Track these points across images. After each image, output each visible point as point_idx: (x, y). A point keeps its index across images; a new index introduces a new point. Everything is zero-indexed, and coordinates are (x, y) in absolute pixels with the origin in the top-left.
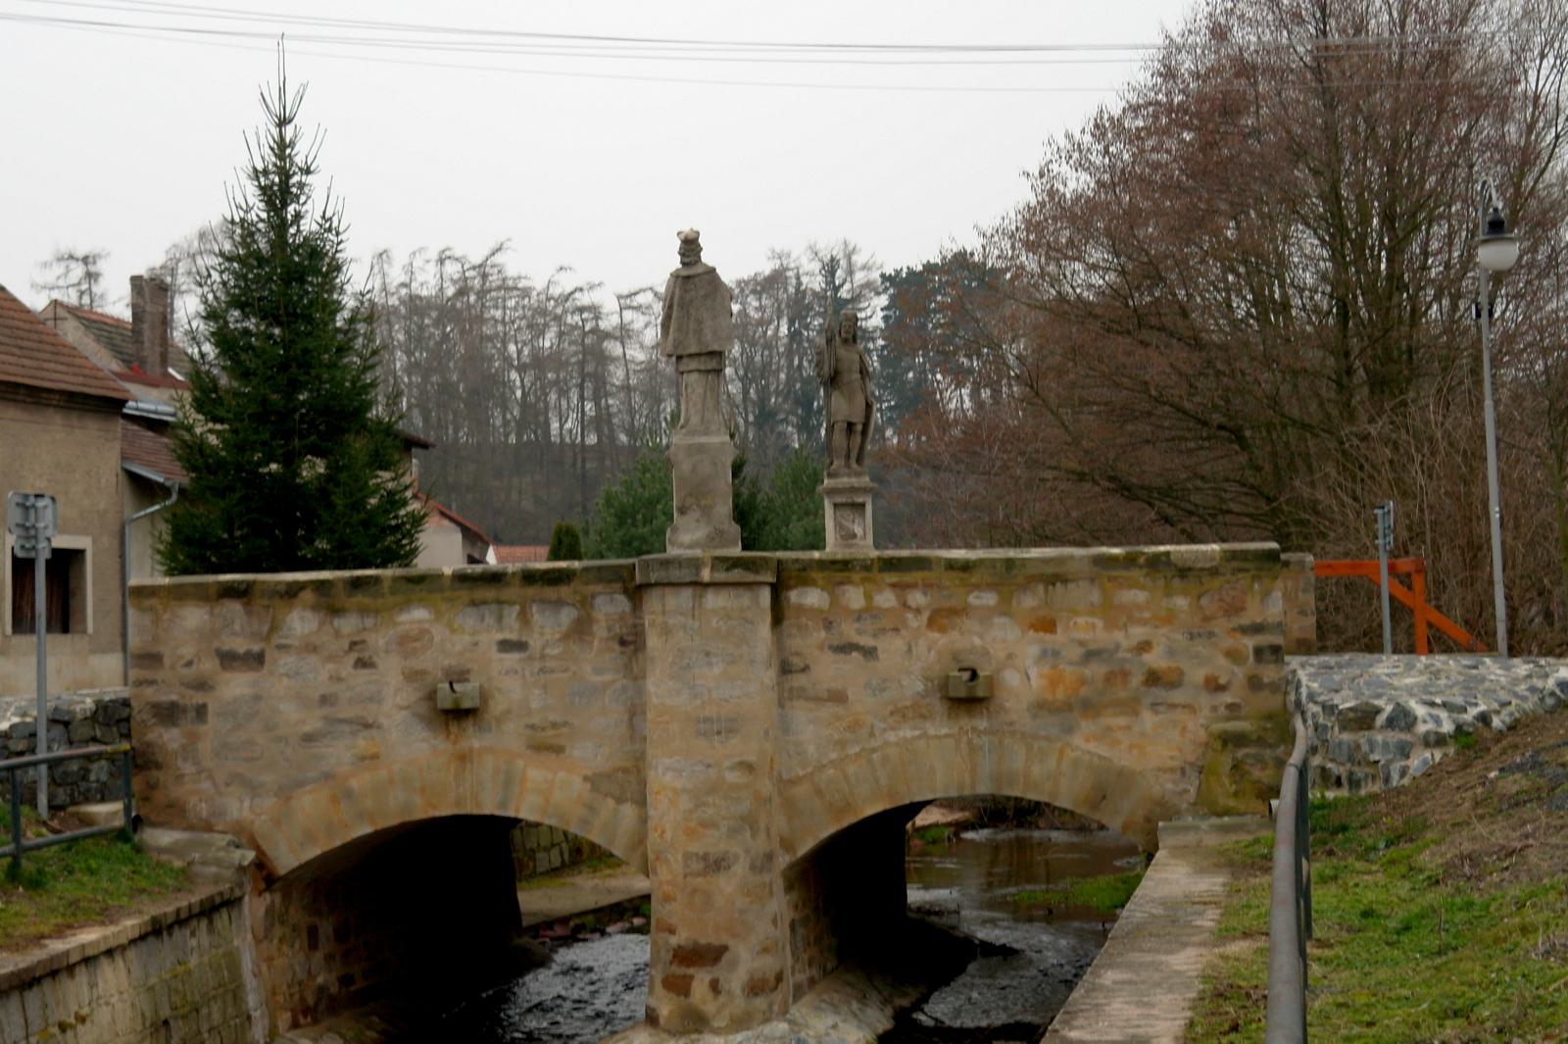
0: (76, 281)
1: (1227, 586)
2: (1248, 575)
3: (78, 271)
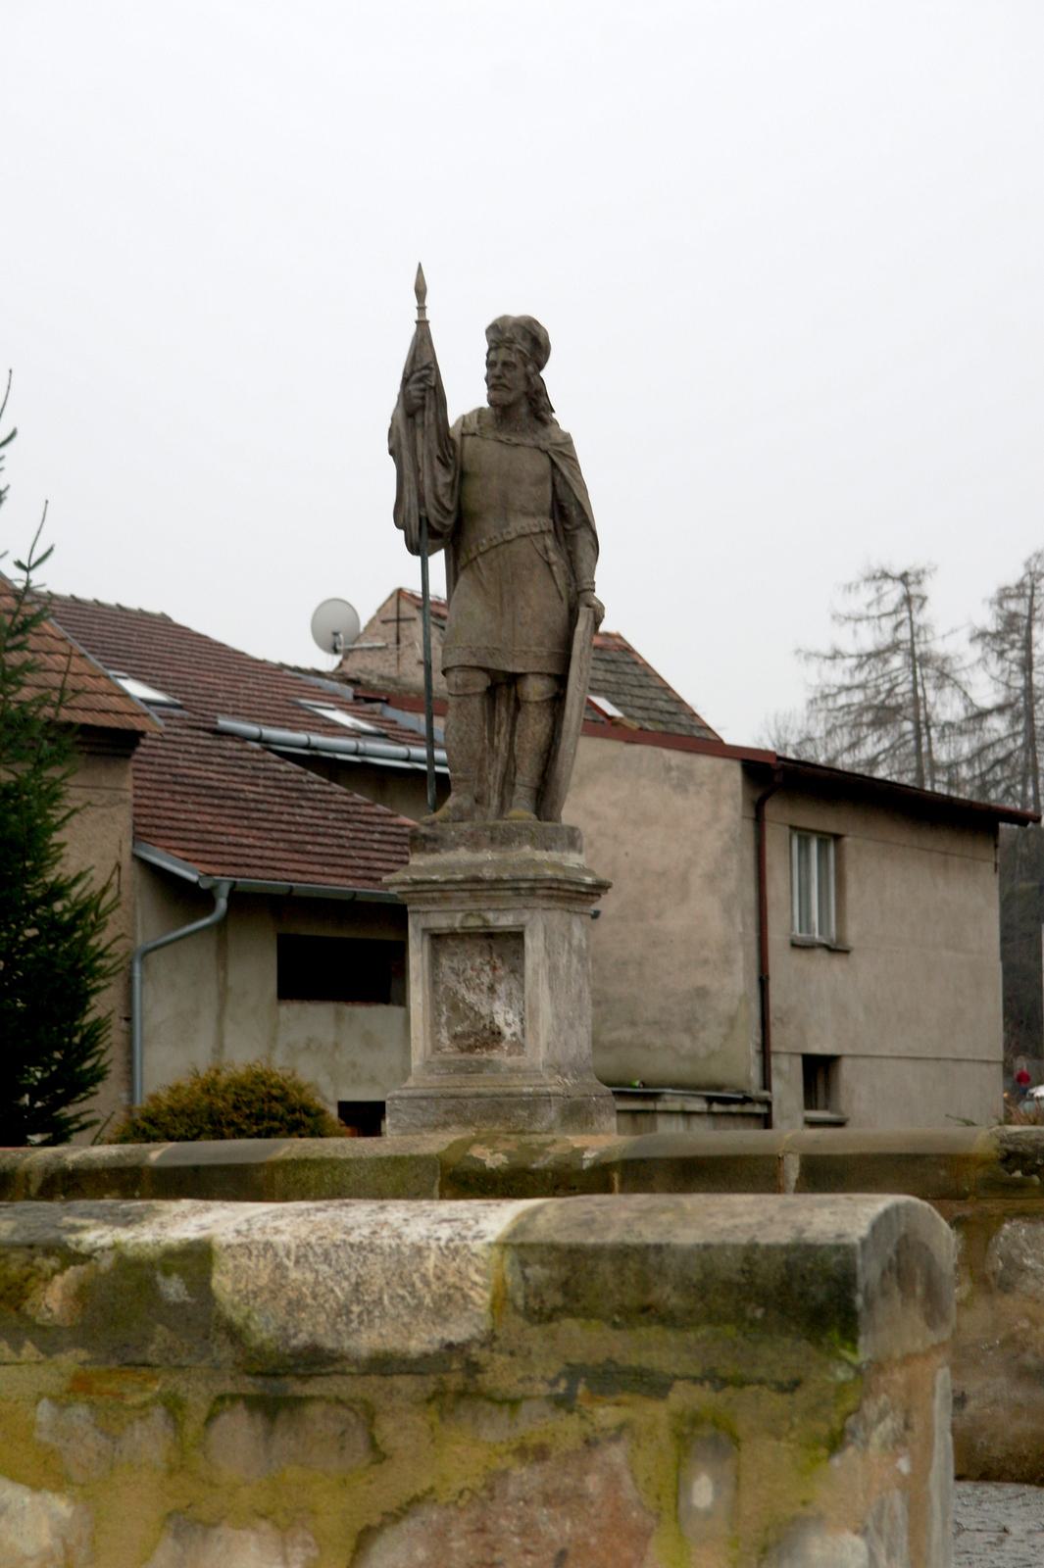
0: (890, 608)
1: (526, 1477)
2: (657, 1413)
3: (894, 593)
